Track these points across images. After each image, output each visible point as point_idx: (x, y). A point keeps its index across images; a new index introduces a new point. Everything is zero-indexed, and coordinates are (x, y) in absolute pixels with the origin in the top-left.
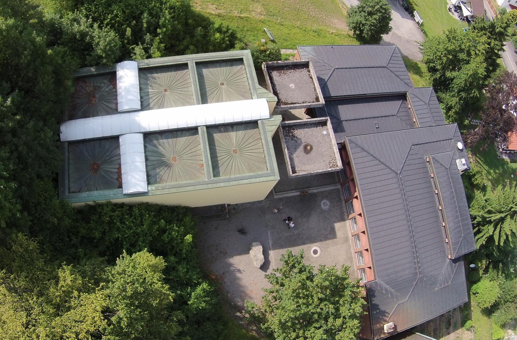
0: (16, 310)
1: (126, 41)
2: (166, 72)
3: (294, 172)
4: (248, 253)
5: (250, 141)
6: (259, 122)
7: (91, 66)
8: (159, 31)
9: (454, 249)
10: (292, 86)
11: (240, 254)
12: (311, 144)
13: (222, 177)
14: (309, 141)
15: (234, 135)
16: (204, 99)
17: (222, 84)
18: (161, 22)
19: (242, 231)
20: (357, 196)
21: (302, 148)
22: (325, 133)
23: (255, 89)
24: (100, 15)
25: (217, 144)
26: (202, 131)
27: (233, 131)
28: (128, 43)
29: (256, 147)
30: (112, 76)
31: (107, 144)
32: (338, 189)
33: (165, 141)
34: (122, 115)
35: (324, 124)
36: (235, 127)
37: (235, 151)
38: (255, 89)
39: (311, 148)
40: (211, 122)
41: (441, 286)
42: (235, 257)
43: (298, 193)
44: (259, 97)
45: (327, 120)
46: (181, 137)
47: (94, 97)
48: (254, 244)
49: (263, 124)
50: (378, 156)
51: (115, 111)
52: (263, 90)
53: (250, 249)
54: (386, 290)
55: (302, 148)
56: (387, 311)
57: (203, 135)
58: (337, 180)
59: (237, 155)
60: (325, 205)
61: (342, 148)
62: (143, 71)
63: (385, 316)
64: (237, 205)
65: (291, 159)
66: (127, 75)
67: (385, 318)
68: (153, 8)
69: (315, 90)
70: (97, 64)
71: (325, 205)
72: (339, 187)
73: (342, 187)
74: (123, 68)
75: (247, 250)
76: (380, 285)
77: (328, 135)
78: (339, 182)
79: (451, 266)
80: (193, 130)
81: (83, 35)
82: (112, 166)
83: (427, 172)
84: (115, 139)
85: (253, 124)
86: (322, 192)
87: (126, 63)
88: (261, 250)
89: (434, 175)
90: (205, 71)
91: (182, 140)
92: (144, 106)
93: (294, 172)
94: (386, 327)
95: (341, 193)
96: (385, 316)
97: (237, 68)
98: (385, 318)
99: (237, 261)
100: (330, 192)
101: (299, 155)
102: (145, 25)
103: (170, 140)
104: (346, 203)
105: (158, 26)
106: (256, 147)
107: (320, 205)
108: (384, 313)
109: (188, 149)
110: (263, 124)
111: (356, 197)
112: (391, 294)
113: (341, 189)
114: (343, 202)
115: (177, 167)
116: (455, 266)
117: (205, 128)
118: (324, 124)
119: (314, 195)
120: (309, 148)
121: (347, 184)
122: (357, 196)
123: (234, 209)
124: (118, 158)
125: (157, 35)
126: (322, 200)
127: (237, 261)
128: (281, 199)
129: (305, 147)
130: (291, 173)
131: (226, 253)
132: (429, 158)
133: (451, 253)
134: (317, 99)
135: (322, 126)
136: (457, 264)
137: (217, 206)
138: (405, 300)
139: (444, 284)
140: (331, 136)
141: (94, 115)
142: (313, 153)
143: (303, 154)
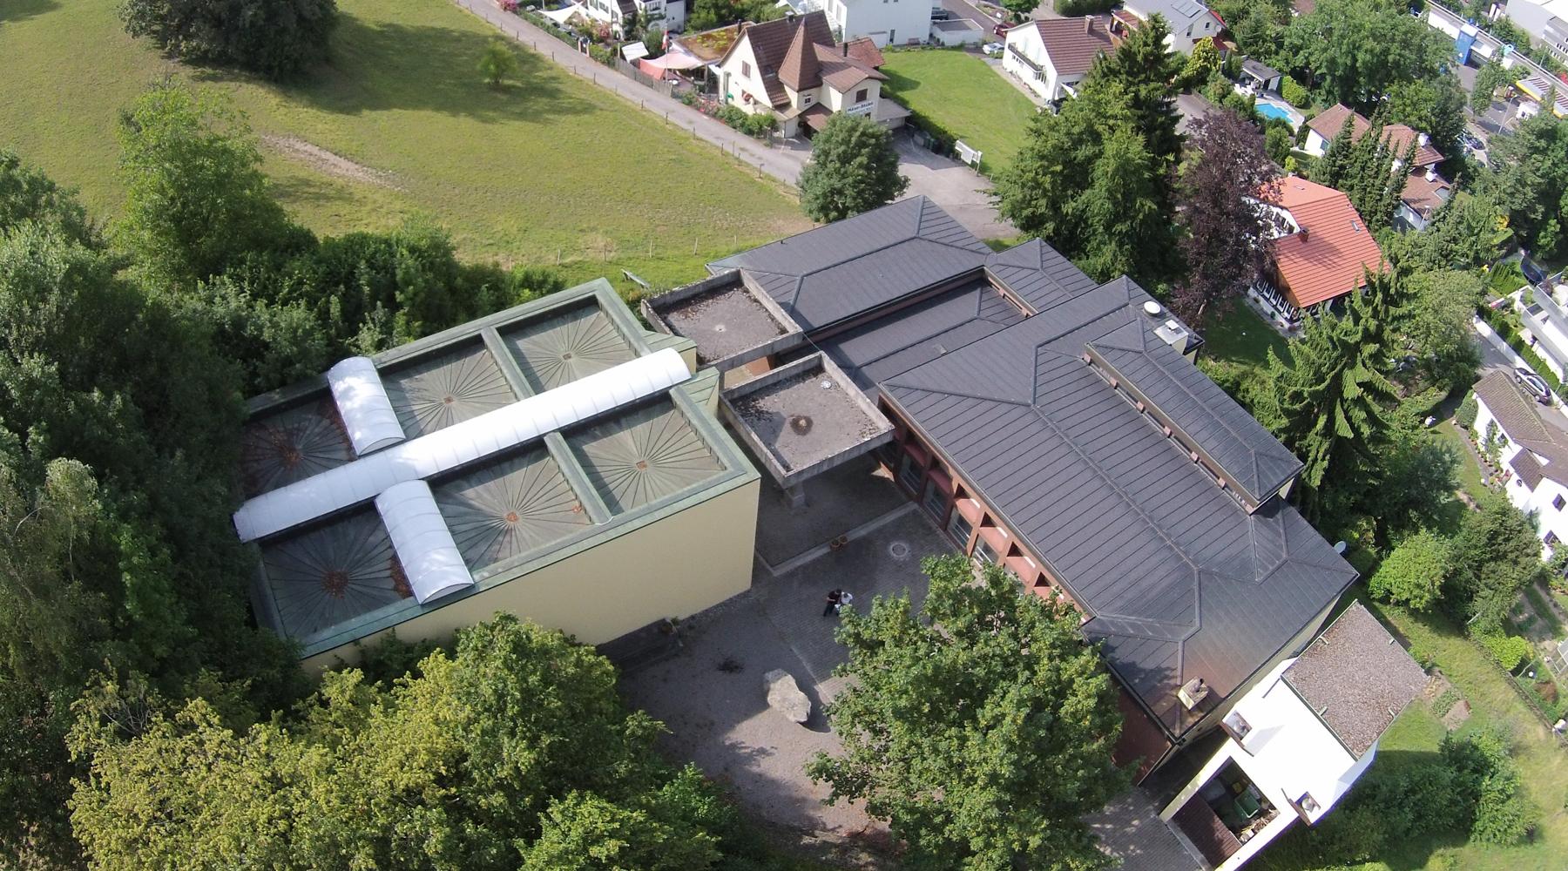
0: (136, 34)
1: (333, 331)
2: (438, 366)
3: (788, 468)
4: (765, 706)
5: (666, 436)
6: (671, 392)
7: (271, 389)
8: (399, 297)
9: (1248, 484)
10: (720, 328)
11: (748, 714)
12: (810, 414)
13: (629, 512)
14: (798, 411)
15: (629, 439)
16: (538, 387)
17: (568, 357)
18: (399, 274)
19: (729, 667)
20: (960, 487)
21: (787, 427)
22: (826, 384)
23: (639, 339)
24: (265, 287)
25: (595, 461)
26: (555, 441)
27: (621, 429)
28: (339, 335)
29: (684, 442)
30: (324, 400)
31: (351, 530)
32: (915, 512)
33: (480, 488)
34: (370, 459)
35: (818, 369)
36: (623, 421)
37: (642, 464)
38: (639, 339)
39: (809, 422)
40: (569, 417)
41: (1266, 569)
42: (738, 727)
43: (825, 550)
44: (654, 348)
45: (820, 358)
46: (512, 471)
47: (292, 450)
48: (769, 675)
49: (682, 393)
50: (968, 392)
51: (350, 454)
52: (658, 337)
53: (765, 694)
54: (1133, 625)
55: (787, 427)
56: (1164, 666)
57: (559, 448)
58: (904, 497)
59: (650, 469)
60: (899, 550)
61: (886, 409)
62: (389, 374)
63: (1167, 677)
64: (693, 617)
65: (775, 454)
66: (357, 387)
67: (1172, 682)
68: (373, 255)
69: (773, 319)
70: (283, 384)
71: (899, 550)
72: (916, 506)
73: (921, 504)
74: (341, 378)
75: (759, 703)
76: (1112, 623)
77: (836, 386)
78: (910, 498)
79: (1268, 525)
80: (533, 449)
81: (239, 323)
82: (376, 568)
83: (1099, 381)
84: (366, 510)
85: (659, 402)
86: (880, 531)
87: (345, 363)
88: (793, 682)
89: (1116, 377)
90: (522, 344)
91: (518, 478)
92: (412, 429)
93: (788, 468)
94: (1183, 695)
95: (925, 516)
96: (1167, 677)
97: (588, 321)
98: (1172, 682)
99: (748, 734)
100: (899, 523)
101: (786, 439)
102: (366, 289)
103: (491, 484)
104: (945, 530)
105: (395, 286)
106: (684, 442)
107: (888, 556)
108: (1160, 673)
109: (534, 491)
110: (682, 393)
111: (961, 493)
112: (1151, 627)
113: (920, 510)
114: (940, 531)
115: (523, 528)
116: (1277, 522)
117: (559, 436)
118: (818, 369)
119: (864, 544)
120: (803, 422)
121: (930, 487)
122: (960, 487)
123: (691, 628)
124: (382, 536)
125: (399, 306)
126: (888, 543)
127: (748, 734)
128: (791, 575)
129: (795, 424)
130: (783, 472)
131: (712, 724)
132: (1090, 353)
133: (1244, 497)
134: (784, 331)
135: (816, 375)
136: (1279, 516)
137: (647, 629)
138: (1192, 630)
139: (1273, 563)
140: (842, 384)
141: (300, 478)
142: (817, 429)
143: (794, 437)
